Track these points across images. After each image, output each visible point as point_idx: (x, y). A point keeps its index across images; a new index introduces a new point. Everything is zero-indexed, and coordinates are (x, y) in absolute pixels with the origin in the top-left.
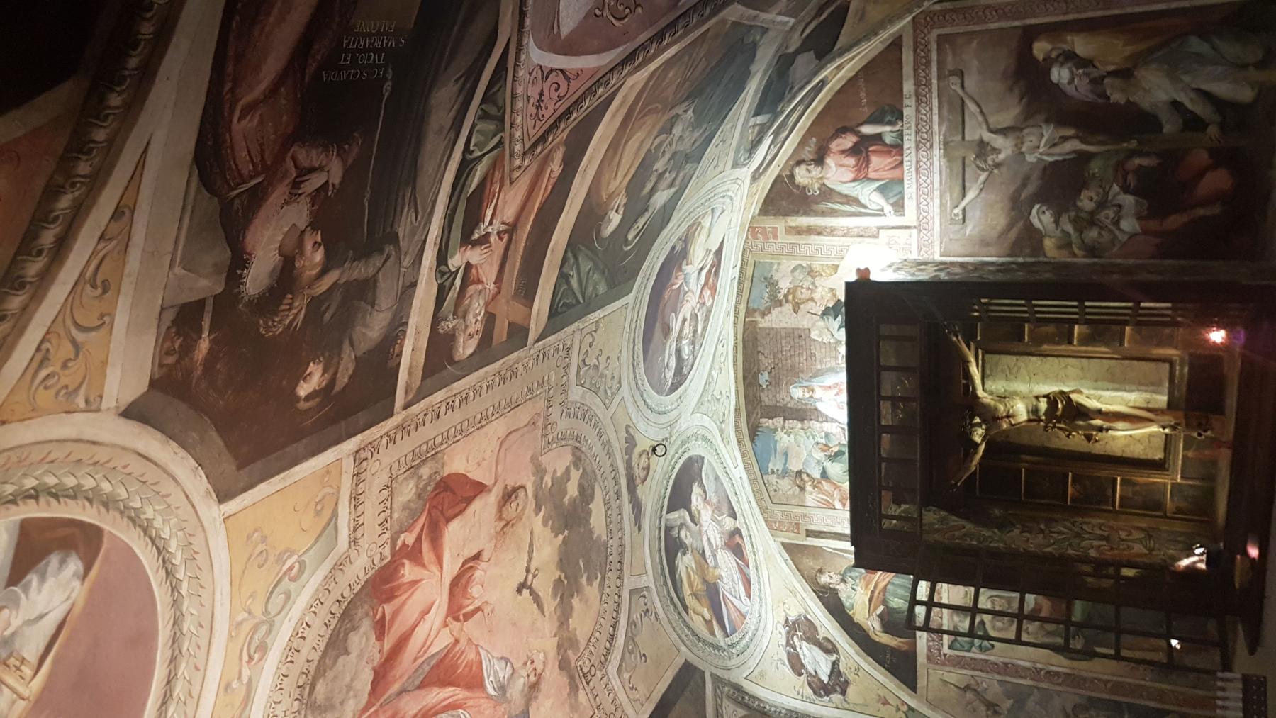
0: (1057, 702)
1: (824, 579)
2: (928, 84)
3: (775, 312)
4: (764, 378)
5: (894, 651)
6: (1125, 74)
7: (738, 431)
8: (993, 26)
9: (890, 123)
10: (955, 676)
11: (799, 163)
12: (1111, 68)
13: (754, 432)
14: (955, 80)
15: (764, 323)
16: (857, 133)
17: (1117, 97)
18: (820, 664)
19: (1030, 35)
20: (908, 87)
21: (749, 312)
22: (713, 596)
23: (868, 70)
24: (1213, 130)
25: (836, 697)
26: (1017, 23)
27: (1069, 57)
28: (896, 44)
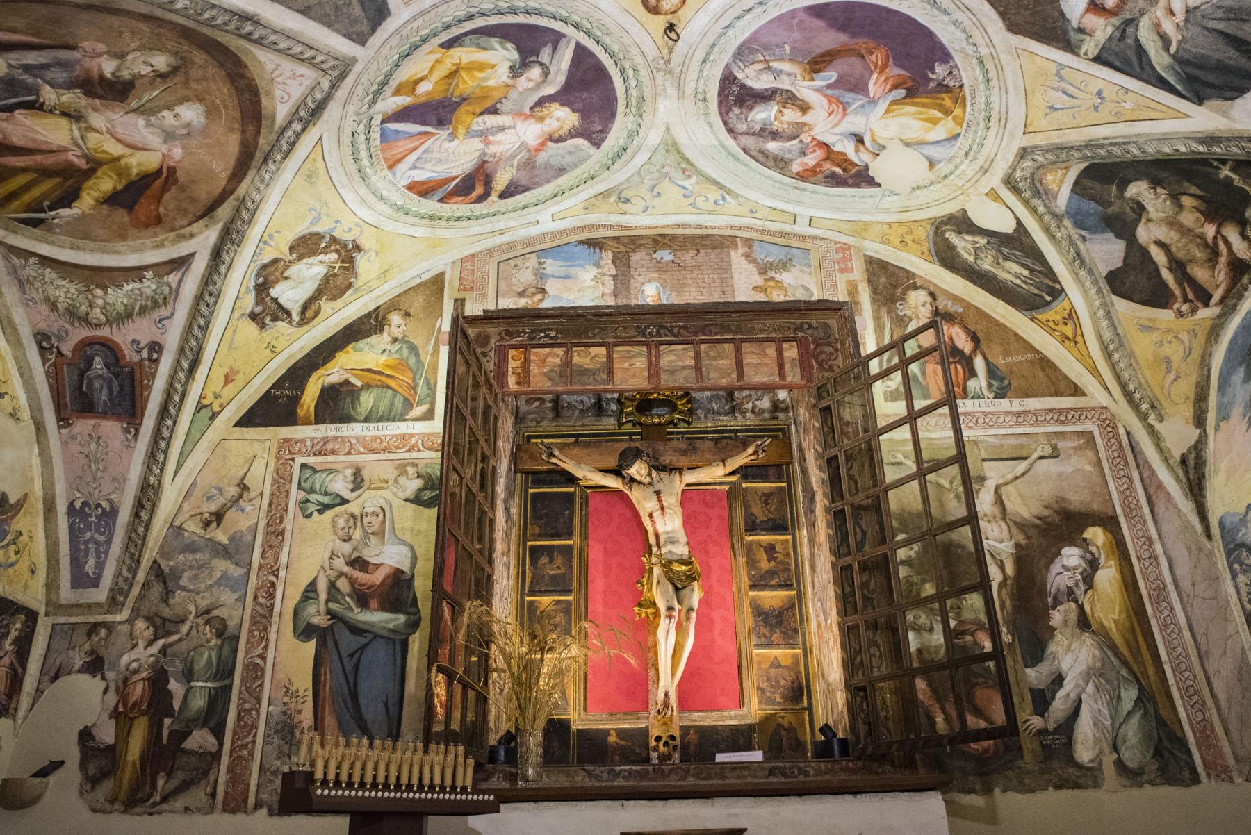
0: (228, 597)
1: (395, 318)
2: (1037, 423)
3: (751, 268)
4: (665, 255)
5: (295, 401)
6: (1084, 623)
7: (593, 227)
8: (1111, 485)
9: (990, 386)
10: (261, 476)
11: (933, 295)
12: (1087, 608)
13: (594, 244)
14: (1048, 450)
15: (736, 256)
16: (974, 351)
17: (1056, 617)
18: (290, 294)
19: (1109, 523)
20: (1033, 404)
21: (748, 242)
22: (437, 113)
23: (1045, 364)
24: (1037, 722)
25: (249, 302)
26: (1119, 510)
27: (1094, 565)
28: (1077, 391)
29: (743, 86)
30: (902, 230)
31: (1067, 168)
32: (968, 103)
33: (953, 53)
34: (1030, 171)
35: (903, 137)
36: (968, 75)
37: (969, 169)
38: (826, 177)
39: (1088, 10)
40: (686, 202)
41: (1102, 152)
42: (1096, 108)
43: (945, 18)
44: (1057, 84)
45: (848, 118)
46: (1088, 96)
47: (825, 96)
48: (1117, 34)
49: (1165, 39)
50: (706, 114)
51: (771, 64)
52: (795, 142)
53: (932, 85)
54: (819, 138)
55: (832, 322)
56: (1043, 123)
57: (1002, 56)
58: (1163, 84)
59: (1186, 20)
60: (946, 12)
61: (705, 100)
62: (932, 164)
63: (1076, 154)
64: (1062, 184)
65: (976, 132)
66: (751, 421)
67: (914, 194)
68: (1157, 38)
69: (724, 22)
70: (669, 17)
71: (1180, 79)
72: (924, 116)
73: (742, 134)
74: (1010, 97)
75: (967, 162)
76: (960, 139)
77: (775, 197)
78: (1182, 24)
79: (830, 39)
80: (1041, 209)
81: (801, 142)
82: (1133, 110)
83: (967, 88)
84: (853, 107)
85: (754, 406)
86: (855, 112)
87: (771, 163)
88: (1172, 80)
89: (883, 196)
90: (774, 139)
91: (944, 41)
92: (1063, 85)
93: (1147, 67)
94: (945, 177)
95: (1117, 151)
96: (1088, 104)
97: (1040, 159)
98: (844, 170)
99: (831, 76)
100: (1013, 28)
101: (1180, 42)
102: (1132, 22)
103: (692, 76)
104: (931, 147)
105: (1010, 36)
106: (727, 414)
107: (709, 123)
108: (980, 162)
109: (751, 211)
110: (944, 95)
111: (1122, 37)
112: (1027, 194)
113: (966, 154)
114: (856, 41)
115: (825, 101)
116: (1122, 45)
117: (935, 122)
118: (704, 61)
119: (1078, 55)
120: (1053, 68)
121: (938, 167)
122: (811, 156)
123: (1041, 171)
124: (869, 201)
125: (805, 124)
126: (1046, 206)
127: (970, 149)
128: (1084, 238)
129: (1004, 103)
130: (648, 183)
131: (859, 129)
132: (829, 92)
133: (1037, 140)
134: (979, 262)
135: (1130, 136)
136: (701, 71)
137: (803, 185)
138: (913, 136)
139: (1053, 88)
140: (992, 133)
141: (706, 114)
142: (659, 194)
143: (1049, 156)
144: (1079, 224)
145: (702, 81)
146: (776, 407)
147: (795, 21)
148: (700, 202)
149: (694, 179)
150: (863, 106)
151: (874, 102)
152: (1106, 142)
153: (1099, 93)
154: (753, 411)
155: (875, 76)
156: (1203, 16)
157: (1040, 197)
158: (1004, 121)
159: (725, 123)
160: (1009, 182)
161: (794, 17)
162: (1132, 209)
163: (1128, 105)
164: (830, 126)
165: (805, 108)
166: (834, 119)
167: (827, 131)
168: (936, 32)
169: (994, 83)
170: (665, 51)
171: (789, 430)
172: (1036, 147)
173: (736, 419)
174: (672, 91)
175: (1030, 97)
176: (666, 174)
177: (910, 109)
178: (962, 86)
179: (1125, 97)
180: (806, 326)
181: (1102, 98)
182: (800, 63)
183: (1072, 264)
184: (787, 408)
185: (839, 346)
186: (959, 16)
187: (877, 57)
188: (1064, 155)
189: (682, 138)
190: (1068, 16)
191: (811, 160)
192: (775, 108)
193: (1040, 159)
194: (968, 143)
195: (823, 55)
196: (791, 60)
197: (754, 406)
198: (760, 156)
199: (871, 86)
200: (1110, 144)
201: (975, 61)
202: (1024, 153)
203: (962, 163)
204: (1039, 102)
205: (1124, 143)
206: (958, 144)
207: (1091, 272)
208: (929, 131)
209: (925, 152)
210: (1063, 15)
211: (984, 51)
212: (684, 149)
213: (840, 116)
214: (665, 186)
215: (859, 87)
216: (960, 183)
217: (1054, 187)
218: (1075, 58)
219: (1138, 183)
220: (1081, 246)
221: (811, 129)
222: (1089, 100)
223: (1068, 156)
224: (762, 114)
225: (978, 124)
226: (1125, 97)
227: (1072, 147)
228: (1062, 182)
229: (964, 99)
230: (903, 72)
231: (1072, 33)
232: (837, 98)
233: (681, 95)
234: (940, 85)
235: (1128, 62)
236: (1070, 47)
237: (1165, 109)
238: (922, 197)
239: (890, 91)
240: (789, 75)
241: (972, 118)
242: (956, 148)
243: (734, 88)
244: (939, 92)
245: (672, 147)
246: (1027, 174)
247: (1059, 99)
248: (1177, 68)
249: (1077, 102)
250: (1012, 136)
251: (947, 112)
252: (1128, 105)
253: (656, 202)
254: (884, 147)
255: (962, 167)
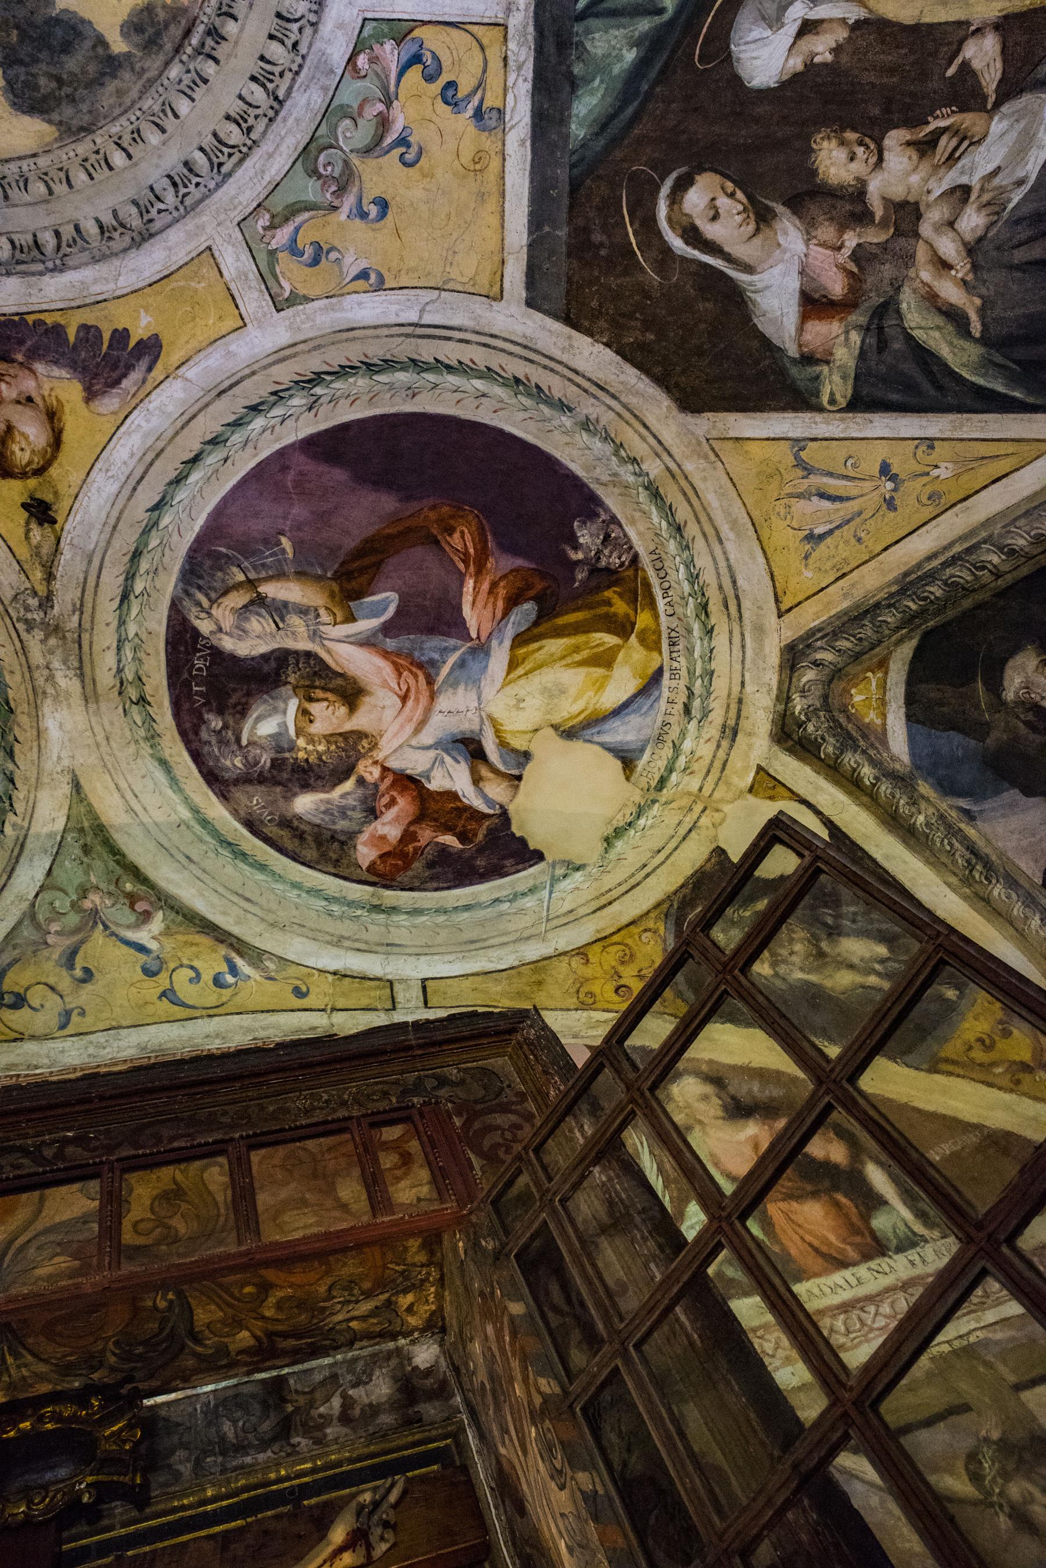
29: (217, 654)
30: (611, 956)
31: (883, 664)
32: (658, 592)
33: (600, 491)
34: (817, 691)
35: (556, 719)
36: (641, 529)
37: (699, 743)
38: (430, 865)
39: (805, 317)
40: (151, 989)
41: (936, 591)
42: (890, 504)
43: (566, 421)
44: (803, 485)
45: (443, 702)
46: (868, 485)
47: (386, 654)
48: (871, 341)
49: (954, 317)
50: (153, 737)
51: (263, 589)
52: (349, 785)
53: (581, 575)
54: (394, 764)
55: (501, 1063)
56: (808, 578)
57: (689, 467)
58: (987, 402)
59: (975, 267)
60: (563, 407)
61: (142, 701)
62: (627, 759)
63: (890, 618)
64: (882, 702)
65: (690, 651)
66: (342, 1446)
67: (612, 855)
68: (939, 320)
69: (147, 496)
70: (32, 482)
71: (1013, 380)
72: (585, 654)
73: (236, 782)
74: (729, 546)
75: (693, 726)
76: (666, 681)
77: (338, 942)
78: (970, 277)
79: (366, 512)
80: (867, 772)
81: (361, 781)
82: (957, 476)
83: (645, 560)
84: (445, 670)
85: (348, 1403)
86: (452, 683)
87: (311, 854)
88: (999, 387)
89: (554, 880)
90: (306, 787)
91: (576, 469)
92: (816, 480)
93: (946, 381)
94: (662, 782)
95: (962, 574)
96: (873, 500)
97: (827, 656)
98: (463, 837)
99: (385, 601)
100: (690, 401)
101: (982, 311)
102: (888, 308)
103: (105, 637)
104: (615, 723)
105: (689, 419)
106: (264, 1445)
107: (163, 763)
108: (717, 717)
109: (299, 993)
110: (608, 594)
111: (882, 345)
112: (829, 749)
113: (687, 710)
114: (415, 505)
115: (386, 668)
116: (888, 357)
117: (604, 660)
118: (125, 597)
119: (820, 409)
120: (783, 454)
121: (641, 764)
122: (390, 815)
123: (838, 686)
124: (529, 902)
125: (361, 735)
126: (873, 763)
127: (691, 694)
128: (967, 813)
129: (722, 564)
130: (59, 945)
131: (468, 724)
132: (390, 644)
133: (811, 616)
134: (782, 969)
135: (972, 533)
136: (122, 623)
137: (390, 897)
138: (576, 708)
139: (799, 496)
140: (720, 641)
141: (153, 737)
142: (87, 970)
143: (843, 644)
144: (948, 788)
145: (128, 653)
146: (411, 1388)
147: (291, 476)
148: (186, 991)
149: (157, 923)
150: (462, 664)
151: (481, 650)
152: (935, 563)
153: (885, 469)
154: (345, 1418)
155: (470, 583)
156: (998, 248)
157: (855, 748)
158: (734, 602)
159: (196, 757)
160: (788, 734)
161: (284, 469)
162: (1027, 723)
163: (944, 472)
164: (409, 729)
165: (351, 694)
166: (414, 709)
167: (407, 744)
168: (557, 454)
169: (692, 529)
170: (38, 575)
171: (462, 1447)
172: (811, 633)
173: (294, 1451)
174: (67, 682)
175: (765, 533)
176: (94, 917)
177: (554, 646)
178: (635, 559)
179: (933, 458)
180: (429, 1084)
181: (894, 478)
182: (319, 578)
183: (967, 881)
184: (444, 1384)
185: (531, 1106)
186: (589, 408)
187: (462, 539)
188: (868, 631)
189: (111, 809)
190: (776, 341)
191: (389, 827)
192: (293, 705)
193: (827, 656)
194: (682, 683)
195: (359, 553)
196: (301, 575)
197: (348, 1403)
198: (284, 836)
199: (467, 611)
200: (945, 565)
201: (643, 496)
202: (793, 656)
203: (683, 734)
204: (783, 536)
205: (969, 551)
206: (666, 693)
207: (1012, 882)
208: (600, 686)
209: (606, 738)
210: (766, 342)
211: (654, 468)
212: (121, 840)
213: (424, 700)
214: (99, 948)
215: (445, 620)
216: (694, 783)
217: (871, 717)
218: (818, 417)
219: (1019, 659)
220: (971, 832)
221: (374, 746)
222: (869, 494)
223: (878, 628)
224: (270, 723)
225: (689, 631)
226: (933, 458)
227: (877, 605)
228: (883, 703)
229: (647, 585)
230: (520, 562)
231: (794, 371)
232: (409, 655)
233: (90, 695)
234: (595, 571)
235: (909, 387)
236: (802, 400)
237: (1010, 448)
238: (631, 851)
239: (506, 613)
240: (303, 611)
241: (674, 623)
242: (663, 704)
243: (199, 664)
244: (599, 589)
245: (92, 837)
246: (814, 699)
247: (816, 513)
248: (999, 359)
249: (853, 506)
250: (760, 630)
251: (623, 628)
252: (944, 472)
253: (85, 996)
254: (527, 755)
255: (687, 745)
